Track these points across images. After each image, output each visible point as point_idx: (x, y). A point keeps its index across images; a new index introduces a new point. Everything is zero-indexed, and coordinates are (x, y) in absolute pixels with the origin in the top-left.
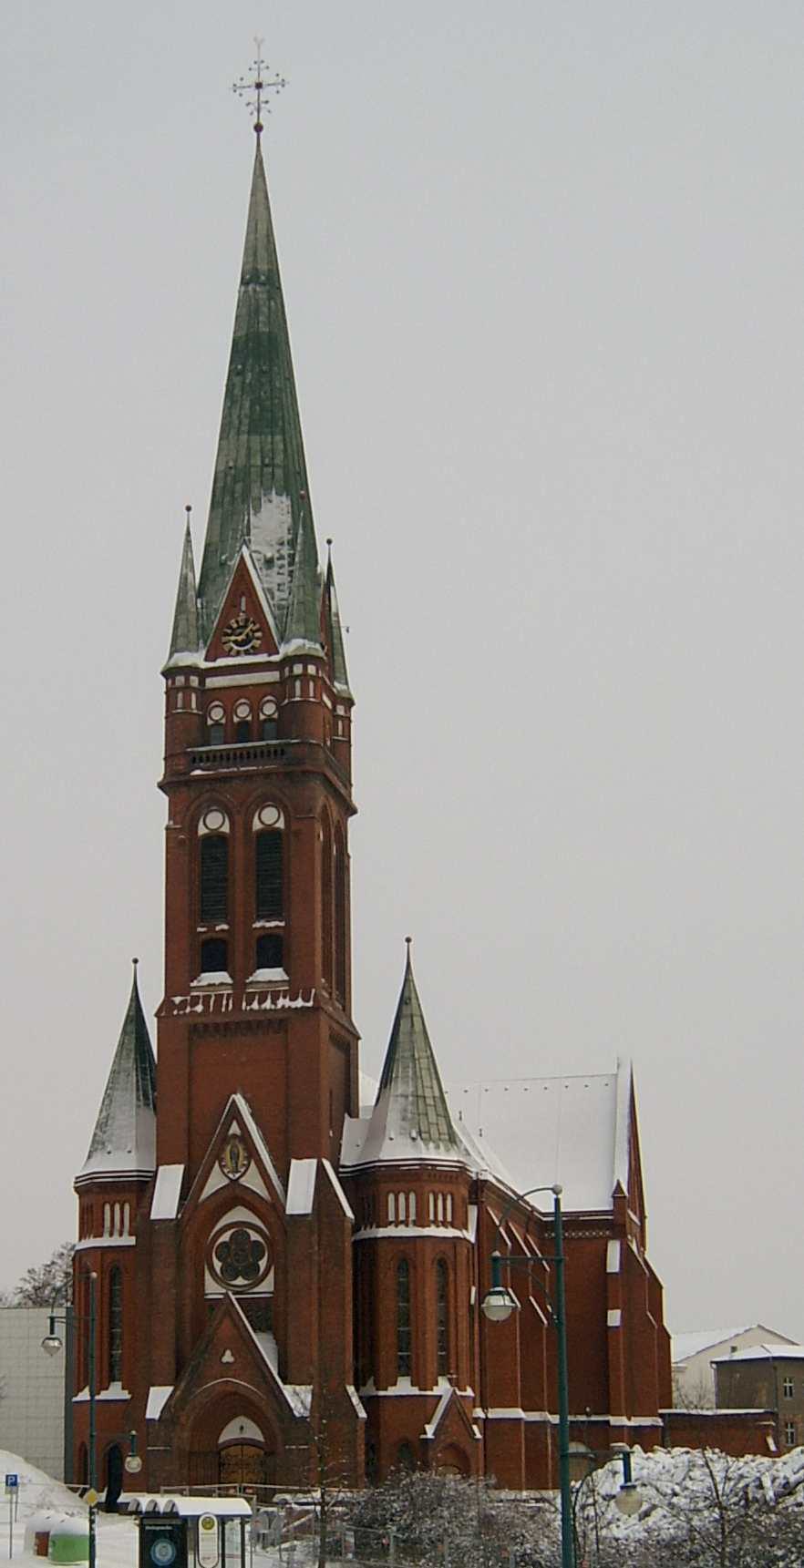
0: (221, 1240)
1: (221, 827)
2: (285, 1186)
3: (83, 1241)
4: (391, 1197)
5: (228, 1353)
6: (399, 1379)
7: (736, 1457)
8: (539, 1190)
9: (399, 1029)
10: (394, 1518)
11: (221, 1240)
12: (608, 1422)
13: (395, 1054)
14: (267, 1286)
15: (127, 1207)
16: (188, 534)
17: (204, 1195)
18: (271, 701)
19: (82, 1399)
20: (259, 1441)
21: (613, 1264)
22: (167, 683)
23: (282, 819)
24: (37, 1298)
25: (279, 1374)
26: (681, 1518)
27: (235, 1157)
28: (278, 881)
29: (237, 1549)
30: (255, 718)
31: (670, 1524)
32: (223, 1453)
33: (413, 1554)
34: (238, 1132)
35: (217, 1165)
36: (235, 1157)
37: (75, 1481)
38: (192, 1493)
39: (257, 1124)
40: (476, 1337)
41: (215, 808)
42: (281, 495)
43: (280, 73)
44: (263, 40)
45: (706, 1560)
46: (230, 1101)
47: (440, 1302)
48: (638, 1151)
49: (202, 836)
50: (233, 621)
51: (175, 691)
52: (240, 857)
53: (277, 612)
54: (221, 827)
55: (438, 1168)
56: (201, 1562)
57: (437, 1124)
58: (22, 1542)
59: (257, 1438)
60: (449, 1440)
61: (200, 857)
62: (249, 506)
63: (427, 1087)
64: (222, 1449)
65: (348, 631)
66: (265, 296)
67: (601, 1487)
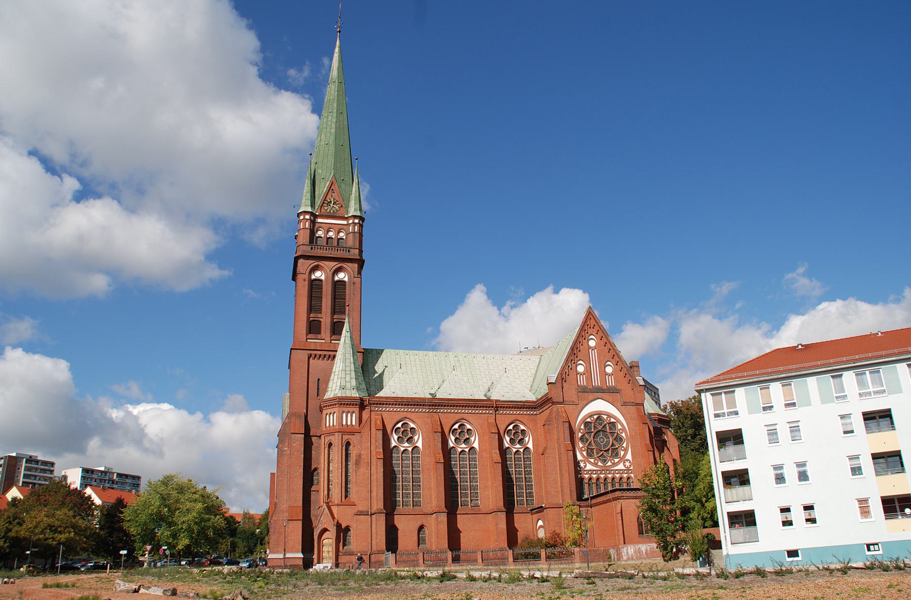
0: (417, 436)
4: (354, 423)
6: (837, 299)
8: (717, 478)
9: (616, 492)
10: (712, 580)
11: (417, 436)
13: (424, 399)
22: (452, 555)
23: (347, 276)
24: (145, 426)
26: (52, 494)
28: (31, 568)
29: (769, 569)
31: (140, 519)
34: (606, 416)
37: (886, 468)
38: (26, 477)
42: (678, 558)
44: (347, 529)
46: (332, 91)
47: (141, 564)
50: (7, 551)
55: (335, 424)
57: (423, 378)
62: (676, 469)
63: (348, 366)
65: (365, 213)
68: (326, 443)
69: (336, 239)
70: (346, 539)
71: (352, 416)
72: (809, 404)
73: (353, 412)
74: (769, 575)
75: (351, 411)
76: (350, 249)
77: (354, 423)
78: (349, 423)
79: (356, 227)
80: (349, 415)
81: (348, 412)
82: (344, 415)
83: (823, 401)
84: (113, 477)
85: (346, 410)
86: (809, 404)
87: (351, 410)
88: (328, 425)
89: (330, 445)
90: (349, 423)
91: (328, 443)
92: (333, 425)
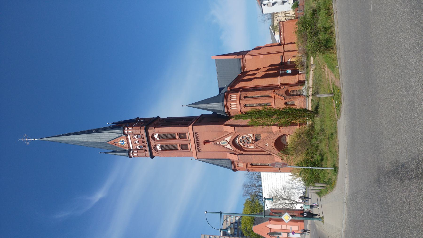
2: (229, 132)
4: (235, 104)
5: (267, 144)
14: (251, 135)
23: (158, 145)
27: (224, 143)
30: (137, 140)
35: (226, 147)
36: (224, 143)
52: (165, 143)
60: (284, 93)
68: (245, 108)
81: (237, 164)
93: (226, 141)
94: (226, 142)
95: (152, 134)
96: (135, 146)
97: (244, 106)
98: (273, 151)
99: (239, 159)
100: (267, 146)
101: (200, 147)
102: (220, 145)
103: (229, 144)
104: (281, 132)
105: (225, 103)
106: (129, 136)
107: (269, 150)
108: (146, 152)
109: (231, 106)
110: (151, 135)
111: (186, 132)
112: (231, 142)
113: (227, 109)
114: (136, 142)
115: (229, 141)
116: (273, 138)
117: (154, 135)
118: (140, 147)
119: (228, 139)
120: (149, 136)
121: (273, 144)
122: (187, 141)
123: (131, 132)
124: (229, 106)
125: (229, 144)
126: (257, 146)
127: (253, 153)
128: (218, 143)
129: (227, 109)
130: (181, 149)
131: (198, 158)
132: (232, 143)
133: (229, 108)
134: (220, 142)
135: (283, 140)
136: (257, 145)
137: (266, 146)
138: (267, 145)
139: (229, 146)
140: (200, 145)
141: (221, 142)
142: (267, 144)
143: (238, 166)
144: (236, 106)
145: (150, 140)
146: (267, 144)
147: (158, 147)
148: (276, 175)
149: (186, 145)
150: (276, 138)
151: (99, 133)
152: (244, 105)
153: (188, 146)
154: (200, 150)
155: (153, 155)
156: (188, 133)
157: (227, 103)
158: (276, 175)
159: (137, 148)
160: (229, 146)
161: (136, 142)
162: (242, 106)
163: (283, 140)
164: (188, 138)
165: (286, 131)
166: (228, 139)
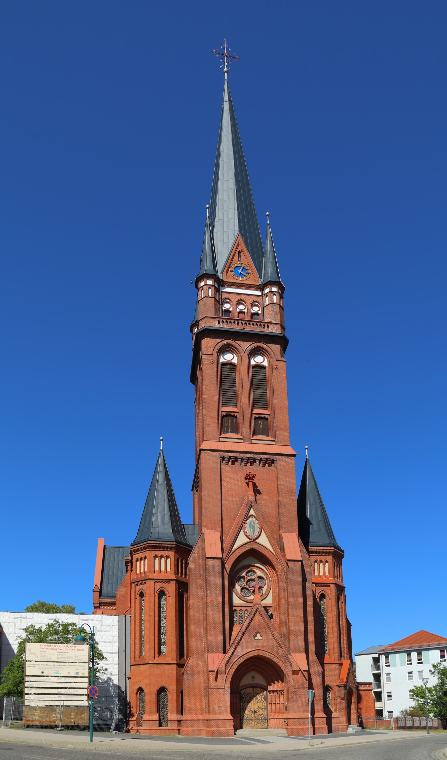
1: (232, 360)
3: (388, 712)
4: (168, 569)
5: (261, 638)
7: (325, 650)
12: (208, 216)
15: (316, 573)
16: (41, 700)
17: (281, 293)
18: (224, 307)
19: (225, 259)
20: (264, 685)
21: (128, 712)
25: (249, 570)
30: (249, 311)
32: (241, 692)
33: (63, 632)
35: (242, 532)
39: (383, 712)
40: (138, 707)
41: (121, 703)
43: (44, 671)
45: (446, 680)
48: (144, 739)
49: (253, 365)
51: (272, 294)
53: (219, 314)
54: (232, 360)
55: (146, 570)
56: (246, 596)
58: (287, 433)
59: (265, 685)
61: (295, 618)
64: (242, 690)
66: (30, 638)
67: (271, 295)
68: (136, 593)
69: (249, 314)
70: (243, 718)
71: (166, 562)
72: (396, 666)
73: (168, 557)
74: (225, 655)
75: (165, 556)
76: (269, 324)
77: (327, 574)
78: (322, 574)
79: (210, 290)
80: (163, 560)
81: (162, 557)
82: (157, 560)
83: (401, 665)
84: (162, 601)
85: (159, 553)
86: (396, 666)
87: (165, 553)
88: (138, 572)
89: (142, 595)
90: (322, 574)
91: (320, 594)
92: (144, 572)
93: (257, 534)
94: (254, 533)
95: (239, 348)
96: (233, 300)
97: (162, 589)
98: (240, 652)
99: (210, 562)
100: (255, 636)
101: (233, 464)
102: (247, 517)
103: (248, 540)
104: (293, 674)
105: (330, 548)
106: (259, 293)
107: (243, 640)
108: (219, 323)
109: (321, 561)
110: (265, 346)
111: (274, 436)
112: (255, 547)
113: (316, 552)
114: (241, 307)
115: (257, 541)
116: (275, 654)
117: (262, 355)
118: (228, 311)
119: (263, 540)
120: (266, 342)
121: (262, 653)
122: (251, 435)
123: (267, 303)
124: (323, 558)
125: (248, 540)
126: (254, 610)
127: (227, 600)
128: (252, 512)
129: (316, 552)
130: (224, 413)
131: (203, 453)
132: (252, 548)
133: (318, 558)
134: (254, 519)
135: (253, 677)
136: (256, 611)
137: (254, 634)
138: (256, 638)
139: (242, 539)
140: (240, 464)
141: (256, 522)
142: (261, 638)
143: (156, 557)
144: (163, 569)
145: (220, 340)
146: (258, 637)
147: (228, 357)
148: (113, 653)
149: (235, 430)
150: (276, 660)
151: (237, 218)
152: (325, 594)
153: (232, 432)
154: (224, 462)
155: (202, 341)
156: (242, 441)
157: (329, 553)
158: (113, 653)
159: (224, 302)
160: (242, 539)
161: (241, 307)
162: (322, 588)
163: (253, 677)
164: (255, 437)
165: (297, 686)
166: (263, 540)
